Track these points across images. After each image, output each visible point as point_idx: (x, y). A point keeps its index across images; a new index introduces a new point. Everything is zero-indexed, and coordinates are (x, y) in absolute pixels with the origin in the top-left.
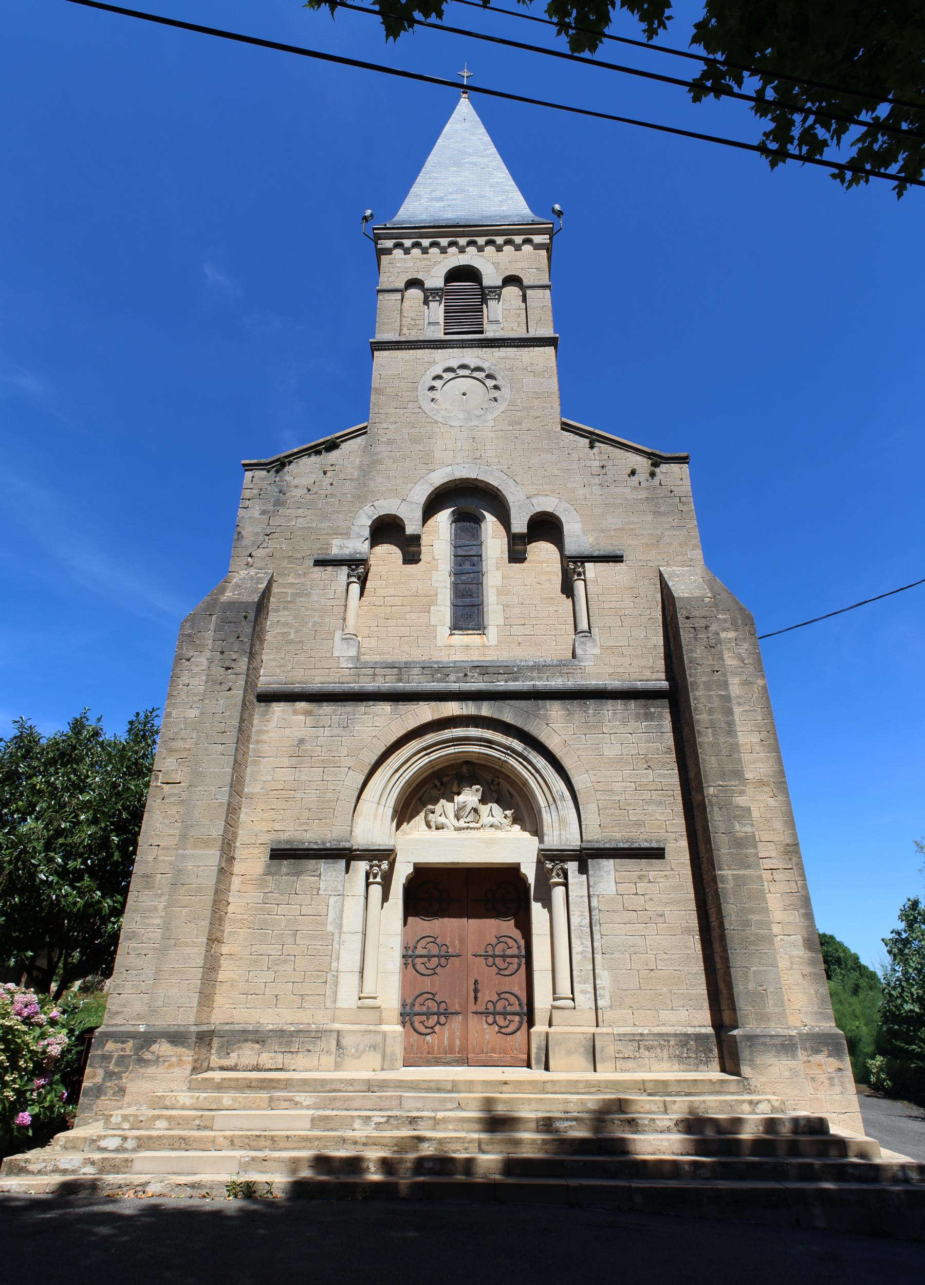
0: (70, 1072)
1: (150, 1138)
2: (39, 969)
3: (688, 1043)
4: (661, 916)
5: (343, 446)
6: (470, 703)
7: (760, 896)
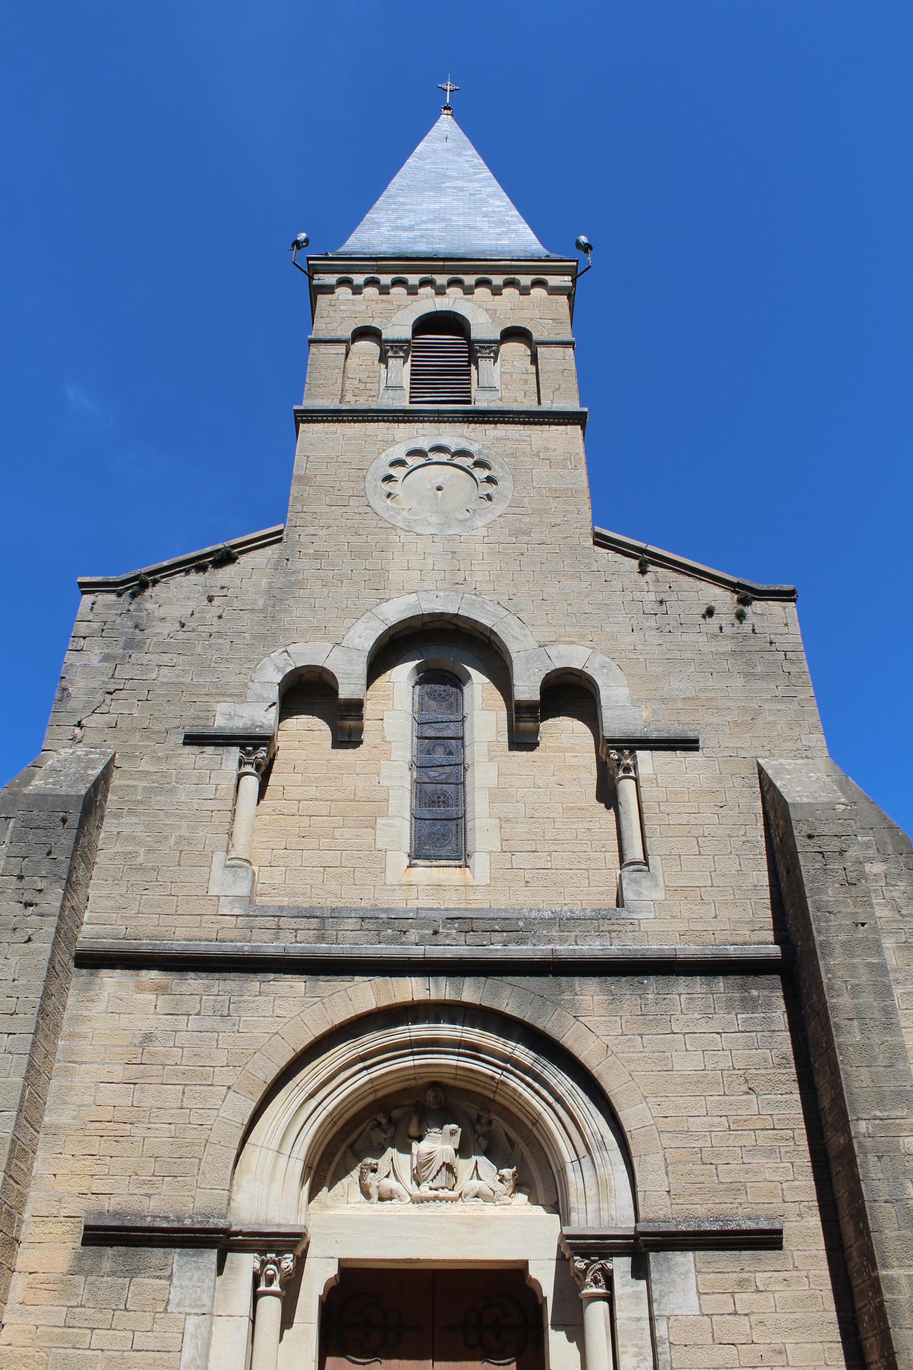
4: (780, 1353)
5: (242, 559)
6: (442, 980)
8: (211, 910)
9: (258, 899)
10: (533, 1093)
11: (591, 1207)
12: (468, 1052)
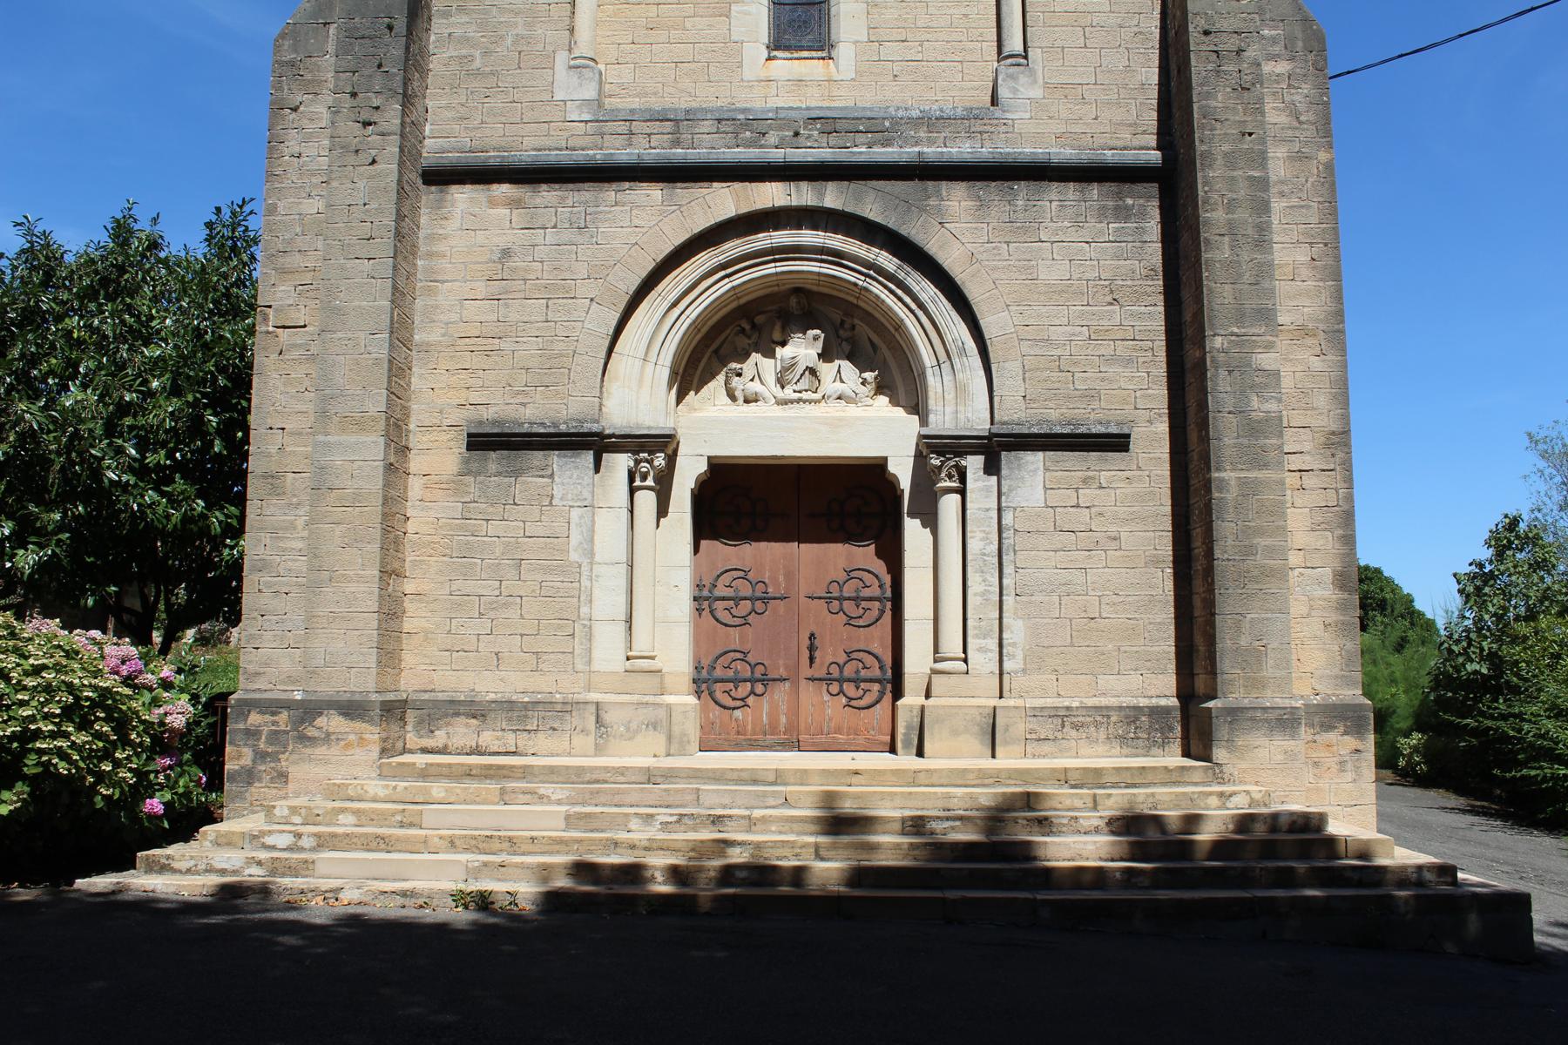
0: (205, 746)
1: (334, 835)
2: (130, 611)
3: (1137, 719)
4: (1115, 539)
6: (804, 185)
7: (1279, 511)
8: (559, 116)
9: (607, 101)
11: (949, 410)
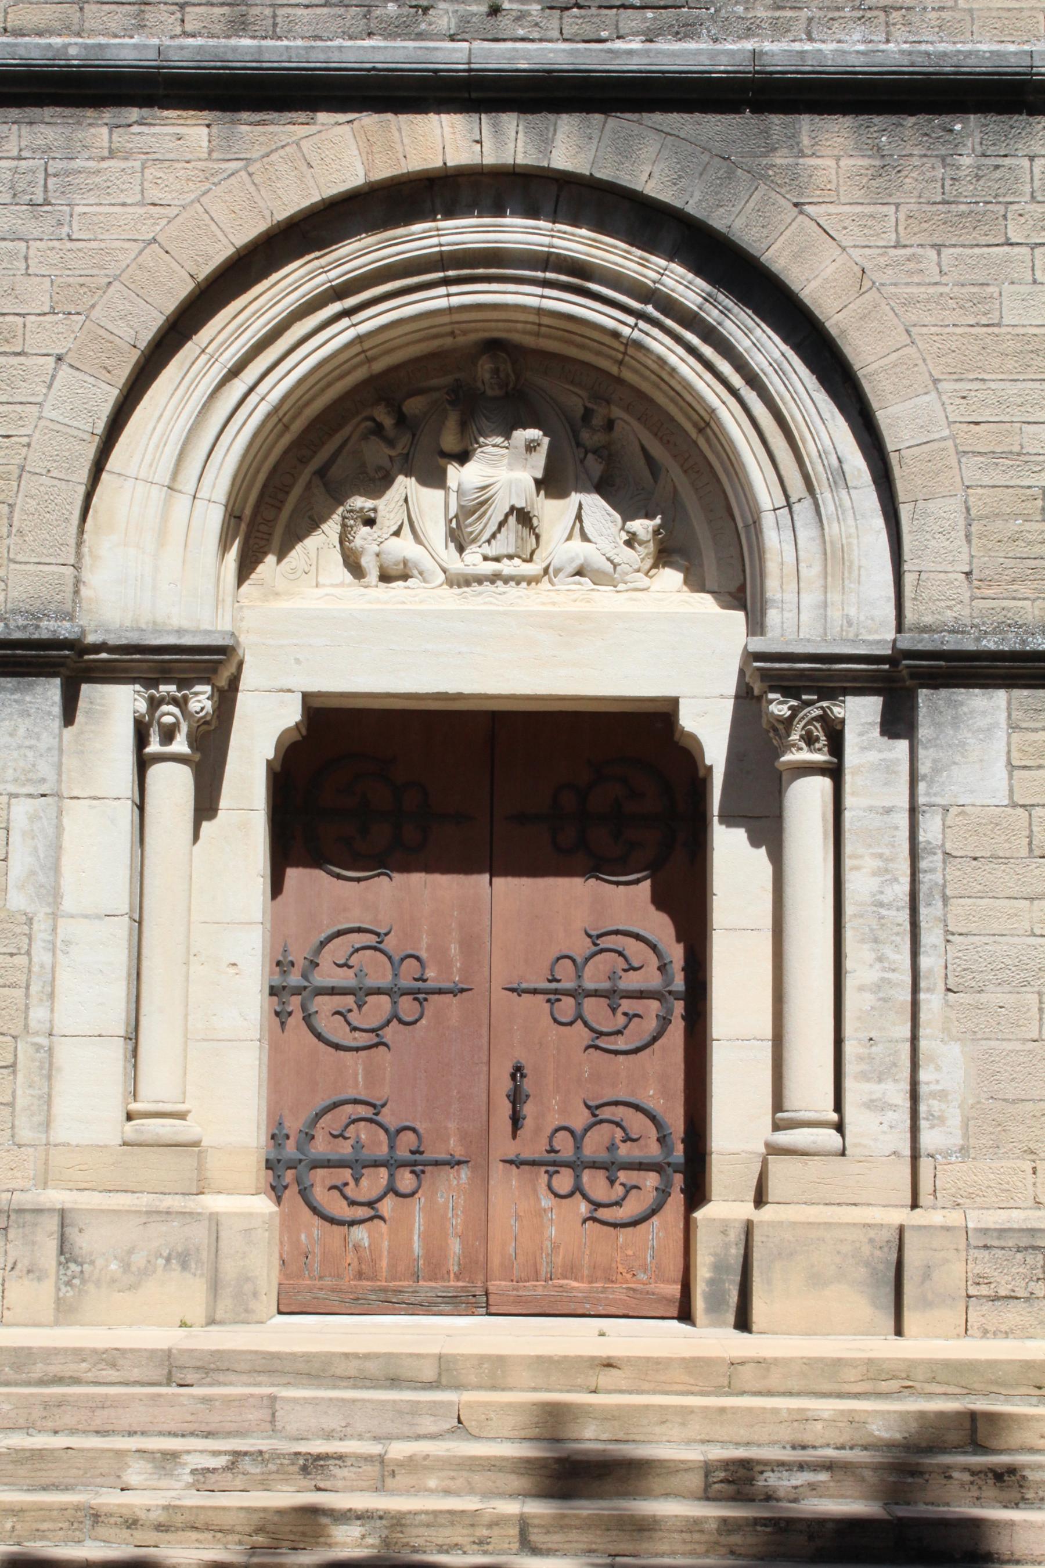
6: (510, 121)
10: (699, 367)
11: (809, 599)
12: (563, 278)
